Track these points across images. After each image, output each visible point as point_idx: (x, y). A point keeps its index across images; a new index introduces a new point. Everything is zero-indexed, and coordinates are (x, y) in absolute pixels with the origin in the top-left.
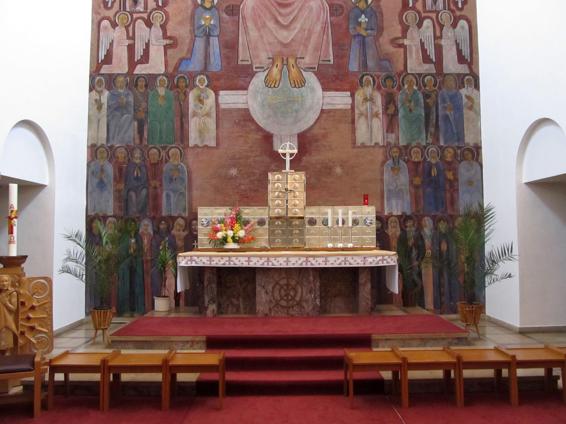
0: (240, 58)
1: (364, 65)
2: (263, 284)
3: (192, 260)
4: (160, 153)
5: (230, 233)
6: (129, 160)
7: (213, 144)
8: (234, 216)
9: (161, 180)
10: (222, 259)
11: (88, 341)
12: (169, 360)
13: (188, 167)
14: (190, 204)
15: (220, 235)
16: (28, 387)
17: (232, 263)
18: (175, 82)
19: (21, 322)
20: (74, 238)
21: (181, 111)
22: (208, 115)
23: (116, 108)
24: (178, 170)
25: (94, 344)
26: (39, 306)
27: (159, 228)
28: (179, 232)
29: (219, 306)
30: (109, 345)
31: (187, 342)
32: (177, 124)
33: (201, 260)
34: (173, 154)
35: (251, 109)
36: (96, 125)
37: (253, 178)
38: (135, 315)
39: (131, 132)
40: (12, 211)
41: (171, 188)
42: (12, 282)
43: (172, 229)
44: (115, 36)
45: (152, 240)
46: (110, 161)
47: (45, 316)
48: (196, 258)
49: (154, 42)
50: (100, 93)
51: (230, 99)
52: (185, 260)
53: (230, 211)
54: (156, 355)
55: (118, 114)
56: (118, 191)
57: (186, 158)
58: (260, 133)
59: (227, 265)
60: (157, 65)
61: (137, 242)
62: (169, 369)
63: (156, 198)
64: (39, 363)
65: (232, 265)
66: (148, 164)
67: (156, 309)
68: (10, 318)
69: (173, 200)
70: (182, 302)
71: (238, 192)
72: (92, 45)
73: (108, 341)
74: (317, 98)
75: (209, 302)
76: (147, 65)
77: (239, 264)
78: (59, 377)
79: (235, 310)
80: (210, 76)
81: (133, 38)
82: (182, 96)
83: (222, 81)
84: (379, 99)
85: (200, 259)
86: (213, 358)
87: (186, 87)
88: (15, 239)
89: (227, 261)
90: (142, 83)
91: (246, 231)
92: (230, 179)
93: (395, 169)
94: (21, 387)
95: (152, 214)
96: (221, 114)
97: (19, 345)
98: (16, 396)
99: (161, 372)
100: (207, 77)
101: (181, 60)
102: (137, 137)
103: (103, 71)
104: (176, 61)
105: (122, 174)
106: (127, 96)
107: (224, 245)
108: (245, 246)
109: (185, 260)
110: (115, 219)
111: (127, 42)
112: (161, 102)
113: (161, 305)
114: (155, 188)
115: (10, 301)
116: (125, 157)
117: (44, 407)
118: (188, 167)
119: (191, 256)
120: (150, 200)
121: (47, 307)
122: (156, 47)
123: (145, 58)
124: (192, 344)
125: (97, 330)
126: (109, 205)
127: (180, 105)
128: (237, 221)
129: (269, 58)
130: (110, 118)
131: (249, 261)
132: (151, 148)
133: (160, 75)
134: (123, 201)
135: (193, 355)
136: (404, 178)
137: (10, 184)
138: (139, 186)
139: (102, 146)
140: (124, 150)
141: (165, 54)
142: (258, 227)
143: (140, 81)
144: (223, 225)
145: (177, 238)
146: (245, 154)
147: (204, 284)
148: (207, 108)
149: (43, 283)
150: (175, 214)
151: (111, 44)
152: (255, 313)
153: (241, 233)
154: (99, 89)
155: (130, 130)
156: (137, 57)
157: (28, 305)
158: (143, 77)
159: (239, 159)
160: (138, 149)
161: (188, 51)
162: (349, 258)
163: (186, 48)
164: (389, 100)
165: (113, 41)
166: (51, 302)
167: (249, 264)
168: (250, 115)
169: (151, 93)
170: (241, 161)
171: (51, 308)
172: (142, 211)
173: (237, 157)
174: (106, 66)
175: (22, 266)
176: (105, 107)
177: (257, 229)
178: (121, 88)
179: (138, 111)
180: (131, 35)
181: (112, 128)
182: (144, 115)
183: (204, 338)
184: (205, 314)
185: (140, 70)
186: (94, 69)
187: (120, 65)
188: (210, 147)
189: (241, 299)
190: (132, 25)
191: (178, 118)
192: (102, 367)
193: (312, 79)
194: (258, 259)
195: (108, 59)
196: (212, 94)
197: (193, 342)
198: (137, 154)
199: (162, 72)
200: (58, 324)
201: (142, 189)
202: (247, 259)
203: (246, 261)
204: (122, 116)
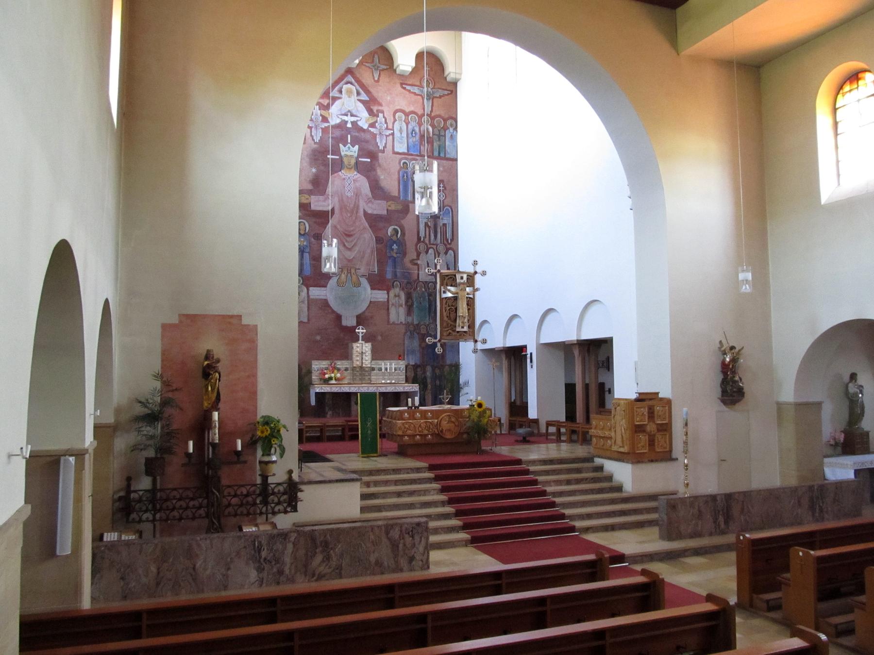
1: (395, 274)
15: (327, 376)
74: (368, 294)
93: (412, 337)
153: (338, 375)
164: (409, 297)
193: (364, 282)
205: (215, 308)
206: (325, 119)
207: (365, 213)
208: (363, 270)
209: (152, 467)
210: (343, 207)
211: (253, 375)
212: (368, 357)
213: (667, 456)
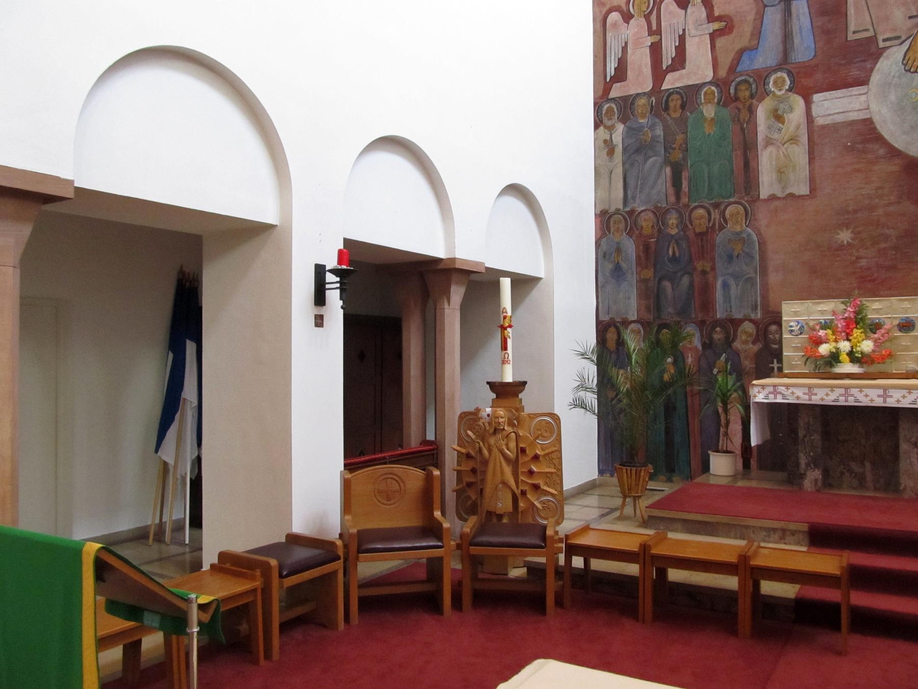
0: (852, 27)
2: (913, 439)
3: (775, 393)
4: (709, 214)
5: (845, 346)
6: (659, 230)
7: (804, 190)
8: (852, 316)
9: (713, 259)
10: (910, 393)
11: (608, 514)
12: (649, 546)
13: (759, 234)
14: (765, 297)
15: (824, 349)
16: (536, 572)
17: (851, 399)
18: (732, 91)
19: (522, 478)
20: (590, 356)
21: (745, 139)
22: (793, 140)
23: (636, 150)
24: (743, 241)
25: (621, 518)
26: (545, 455)
27: (711, 339)
28: (745, 344)
29: (826, 473)
30: (644, 522)
31: (774, 530)
32: (738, 162)
33: (793, 393)
34: (732, 215)
35: (877, 119)
36: (607, 180)
37: (883, 245)
38: (674, 479)
39: (661, 186)
40: (505, 318)
41: (730, 271)
42: (509, 419)
43: (734, 340)
44: (630, 35)
45: (699, 361)
46: (630, 234)
47: (553, 470)
48: (783, 388)
49: (693, 32)
50: (611, 129)
51: (834, 106)
52: (762, 392)
53: (843, 307)
54: (727, 546)
55: (640, 158)
56: (643, 281)
57: (756, 219)
58: (897, 161)
59: (842, 402)
61: (675, 362)
62: (751, 572)
63: (706, 290)
64: (552, 537)
65: (851, 402)
66: (691, 234)
67: (712, 471)
68: (508, 470)
69: (734, 291)
70: (753, 463)
71: (854, 273)
72: (595, 56)
73: (642, 517)
75: (808, 465)
76: (684, 71)
77: (864, 401)
78: (578, 562)
79: (855, 482)
80: (794, 71)
81: (659, 32)
82: (744, 115)
83: (819, 76)
85: (864, 393)
86: (828, 563)
87: (752, 96)
88: (510, 358)
89: (841, 395)
90: (675, 102)
91: (875, 341)
92: (837, 250)
94: (525, 570)
95: (700, 315)
96: (817, 136)
97: (520, 510)
98: (517, 580)
99: (736, 574)
100: (790, 73)
101: (741, 53)
102: (671, 191)
103: (613, 94)
104: (731, 56)
105: (649, 254)
106: (652, 127)
107: (832, 366)
108: (874, 368)
109: (762, 392)
110: (640, 326)
111: (649, 41)
112: (708, 129)
113: (721, 466)
114: (704, 273)
115: (507, 445)
116: (653, 226)
117: (559, 603)
118: (759, 234)
119: (775, 386)
120: (696, 294)
121: (555, 457)
122: (697, 39)
123: (680, 60)
124: (783, 535)
125: (625, 497)
126: (631, 305)
127: (743, 129)
128: (857, 323)
129: (910, 17)
130: (627, 166)
131: (885, 396)
132: (696, 208)
133: (704, 84)
134: (652, 297)
135: (788, 555)
137: (501, 279)
138: (676, 272)
139: (617, 211)
140: (651, 215)
141: (713, 47)
142: (899, 334)
143: (672, 100)
144: (829, 332)
145: (742, 356)
146: (867, 202)
147: (797, 434)
148: (792, 129)
149: (549, 423)
150: (738, 316)
151: (625, 49)
152: (897, 490)
153: (867, 346)
154: (609, 123)
155: (660, 181)
156: (666, 62)
157: (530, 453)
158: (678, 93)
159: (856, 211)
160: (674, 212)
161: (752, 35)
162: (854, 391)
163: (748, 29)
165: (626, 43)
166: (560, 451)
167: (885, 401)
168: (875, 129)
169: (691, 117)
170: (859, 215)
171: (560, 458)
172: (683, 312)
173: (850, 209)
174: (618, 84)
175: (520, 396)
176: (619, 149)
177: (896, 337)
178: (643, 116)
179: (671, 150)
180: (654, 27)
181: (631, 182)
182: (681, 156)
183: (805, 527)
184: (801, 486)
185: (671, 82)
186: (600, 93)
187: (639, 80)
188: (800, 196)
189: (868, 464)
190: (655, 12)
191: (739, 153)
192: (642, 554)
194: (905, 392)
195: (621, 74)
196: (798, 102)
197: (784, 530)
198: (673, 219)
199: (709, 79)
200: (570, 481)
201: (682, 276)
202: (881, 392)
203: (879, 396)
204: (646, 160)
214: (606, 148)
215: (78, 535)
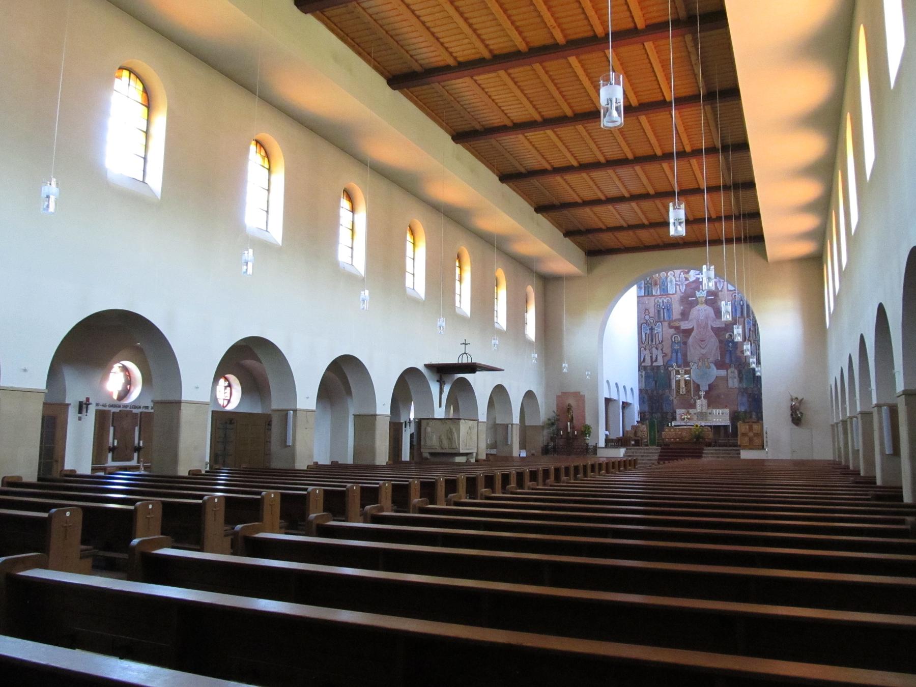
1: (731, 361)
23: (647, 377)
28: (669, 417)
60: (660, 362)
74: (715, 372)
84: (736, 372)
93: (743, 396)
94: (85, 468)
105: (651, 398)
123: (656, 360)
126: (646, 408)
134: (651, 407)
136: (745, 399)
164: (740, 372)
185: (654, 364)
187: (648, 363)
193: (713, 366)
205: (572, 390)
206: (687, 279)
207: (712, 328)
208: (711, 359)
209: (552, 439)
210: (699, 325)
211: (584, 412)
212: (705, 408)
213: (763, 448)
214: (640, 376)
215: (478, 473)
